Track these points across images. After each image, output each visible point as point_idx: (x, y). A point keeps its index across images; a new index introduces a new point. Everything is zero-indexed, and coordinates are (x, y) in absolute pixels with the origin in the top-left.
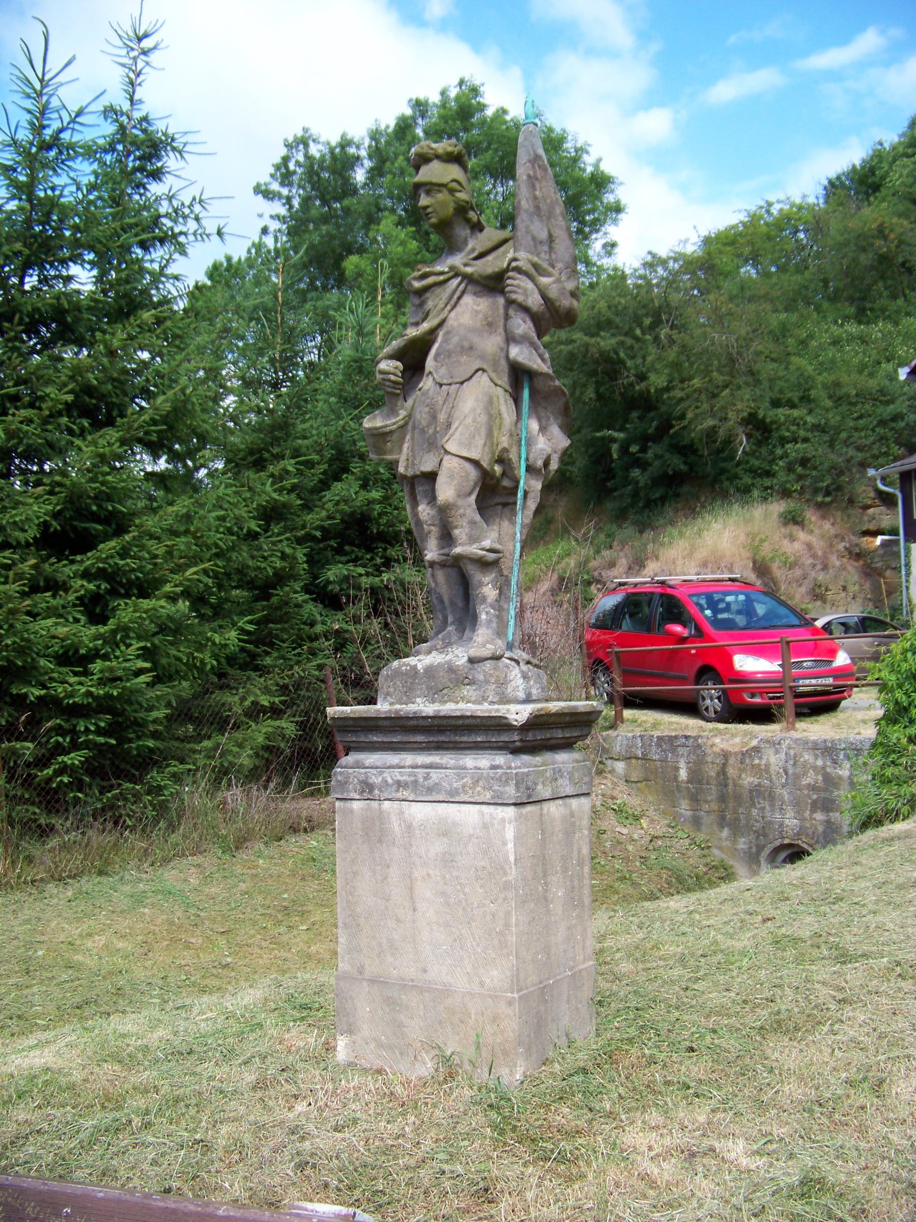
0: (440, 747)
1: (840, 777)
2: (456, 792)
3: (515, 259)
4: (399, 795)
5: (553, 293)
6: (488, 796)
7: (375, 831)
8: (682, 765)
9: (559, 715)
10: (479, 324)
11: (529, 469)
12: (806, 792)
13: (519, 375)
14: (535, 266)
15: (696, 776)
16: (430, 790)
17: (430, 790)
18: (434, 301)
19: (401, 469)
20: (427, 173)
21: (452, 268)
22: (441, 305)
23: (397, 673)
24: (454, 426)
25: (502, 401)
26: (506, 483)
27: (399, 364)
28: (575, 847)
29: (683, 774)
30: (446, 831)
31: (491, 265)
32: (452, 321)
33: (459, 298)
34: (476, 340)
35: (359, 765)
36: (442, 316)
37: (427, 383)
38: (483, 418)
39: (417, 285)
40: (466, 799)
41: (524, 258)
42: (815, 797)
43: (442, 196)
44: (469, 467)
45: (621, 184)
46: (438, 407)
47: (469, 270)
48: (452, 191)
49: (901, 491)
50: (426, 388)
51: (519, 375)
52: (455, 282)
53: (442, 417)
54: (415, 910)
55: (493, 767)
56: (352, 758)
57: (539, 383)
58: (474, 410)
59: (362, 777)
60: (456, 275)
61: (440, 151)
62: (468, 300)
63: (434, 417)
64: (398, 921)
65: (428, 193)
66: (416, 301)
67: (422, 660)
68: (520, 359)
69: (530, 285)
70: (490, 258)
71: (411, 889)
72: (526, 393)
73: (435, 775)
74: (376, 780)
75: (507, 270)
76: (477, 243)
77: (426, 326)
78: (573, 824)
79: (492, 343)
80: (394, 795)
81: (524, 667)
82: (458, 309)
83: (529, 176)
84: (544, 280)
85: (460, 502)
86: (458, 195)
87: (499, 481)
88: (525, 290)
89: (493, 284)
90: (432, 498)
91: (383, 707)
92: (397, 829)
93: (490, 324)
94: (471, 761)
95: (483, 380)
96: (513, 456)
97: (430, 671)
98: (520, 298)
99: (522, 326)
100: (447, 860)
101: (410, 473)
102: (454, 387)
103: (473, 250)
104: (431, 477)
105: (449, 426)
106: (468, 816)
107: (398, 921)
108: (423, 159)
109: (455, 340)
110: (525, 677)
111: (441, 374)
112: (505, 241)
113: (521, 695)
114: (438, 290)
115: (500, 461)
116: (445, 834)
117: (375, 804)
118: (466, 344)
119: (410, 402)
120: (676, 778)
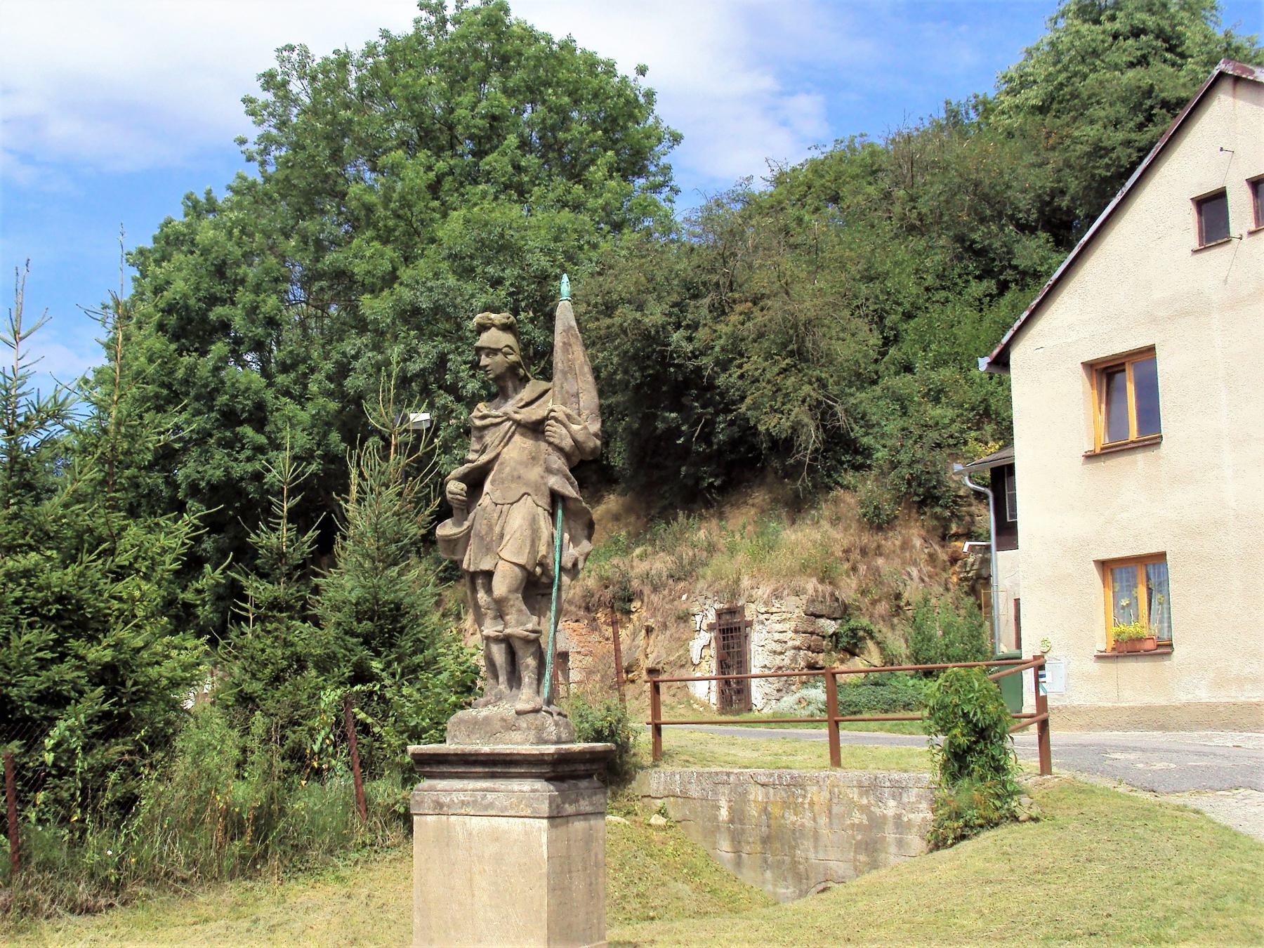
0: (493, 776)
1: (885, 817)
2: (506, 809)
3: (553, 411)
4: (463, 811)
5: (580, 437)
6: (528, 812)
7: (445, 839)
8: (723, 803)
9: (582, 753)
10: (525, 458)
11: (561, 569)
12: (850, 832)
13: (556, 498)
14: (568, 416)
15: (737, 815)
16: (486, 807)
17: (486, 807)
18: (491, 437)
19: (465, 566)
20: (485, 339)
21: (506, 414)
22: (496, 442)
23: (461, 721)
24: (506, 538)
25: (542, 519)
26: (544, 580)
27: (464, 486)
28: (593, 854)
29: (724, 814)
30: (496, 837)
31: (534, 413)
32: (503, 455)
33: (511, 437)
34: (522, 471)
35: (432, 789)
36: (498, 451)
37: (485, 501)
38: (528, 533)
39: (478, 423)
40: (513, 813)
41: (560, 411)
42: (859, 837)
43: (499, 357)
44: (517, 569)
45: (677, 139)
46: (494, 522)
47: (518, 417)
48: (506, 354)
49: (993, 491)
50: (484, 504)
51: (556, 498)
52: (508, 424)
53: (497, 529)
54: (473, 896)
55: (533, 791)
56: (426, 783)
57: (571, 505)
58: (521, 526)
59: (434, 798)
60: (509, 419)
61: (497, 322)
62: (517, 438)
63: (491, 528)
64: (460, 904)
65: (487, 356)
66: (478, 434)
67: (480, 712)
68: (556, 487)
69: (564, 431)
70: (534, 406)
71: (471, 880)
72: (560, 512)
73: (490, 796)
74: (445, 799)
75: (546, 418)
76: (526, 393)
77: (485, 458)
78: (591, 835)
79: (535, 473)
80: (459, 811)
81: (556, 717)
82: (510, 445)
83: (564, 343)
84: (575, 427)
85: (511, 596)
86: (510, 357)
87: (539, 578)
88: (558, 433)
89: (536, 429)
90: (489, 590)
91: (449, 747)
92: (460, 836)
93: (533, 458)
94: (516, 785)
95: (528, 501)
96: (549, 561)
97: (487, 720)
98: (556, 441)
99: (558, 462)
100: (498, 859)
101: (472, 569)
102: (506, 507)
103: (522, 400)
104: (489, 575)
105: (502, 536)
106: (514, 826)
107: (460, 904)
108: (482, 328)
109: (507, 469)
110: (557, 724)
111: (497, 496)
112: (546, 391)
113: (554, 738)
114: (493, 429)
115: (541, 564)
116: (497, 839)
117: (444, 818)
118: (515, 474)
119: (472, 515)
120: (716, 818)
